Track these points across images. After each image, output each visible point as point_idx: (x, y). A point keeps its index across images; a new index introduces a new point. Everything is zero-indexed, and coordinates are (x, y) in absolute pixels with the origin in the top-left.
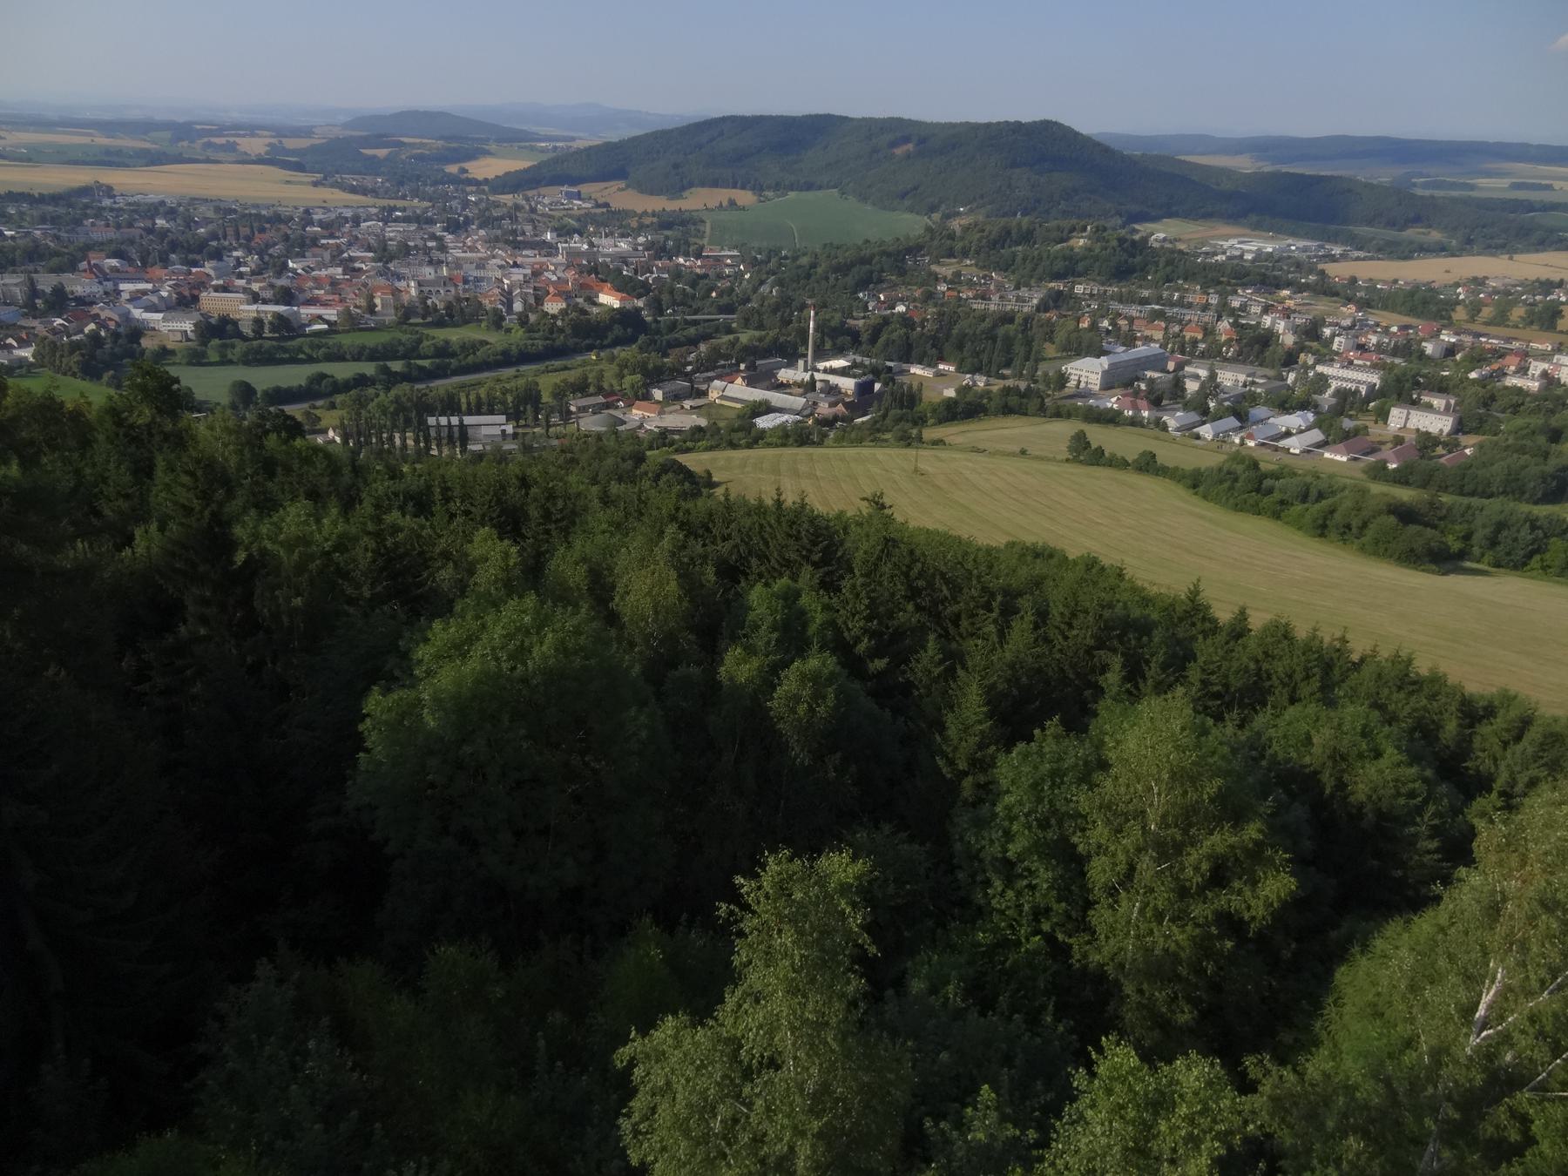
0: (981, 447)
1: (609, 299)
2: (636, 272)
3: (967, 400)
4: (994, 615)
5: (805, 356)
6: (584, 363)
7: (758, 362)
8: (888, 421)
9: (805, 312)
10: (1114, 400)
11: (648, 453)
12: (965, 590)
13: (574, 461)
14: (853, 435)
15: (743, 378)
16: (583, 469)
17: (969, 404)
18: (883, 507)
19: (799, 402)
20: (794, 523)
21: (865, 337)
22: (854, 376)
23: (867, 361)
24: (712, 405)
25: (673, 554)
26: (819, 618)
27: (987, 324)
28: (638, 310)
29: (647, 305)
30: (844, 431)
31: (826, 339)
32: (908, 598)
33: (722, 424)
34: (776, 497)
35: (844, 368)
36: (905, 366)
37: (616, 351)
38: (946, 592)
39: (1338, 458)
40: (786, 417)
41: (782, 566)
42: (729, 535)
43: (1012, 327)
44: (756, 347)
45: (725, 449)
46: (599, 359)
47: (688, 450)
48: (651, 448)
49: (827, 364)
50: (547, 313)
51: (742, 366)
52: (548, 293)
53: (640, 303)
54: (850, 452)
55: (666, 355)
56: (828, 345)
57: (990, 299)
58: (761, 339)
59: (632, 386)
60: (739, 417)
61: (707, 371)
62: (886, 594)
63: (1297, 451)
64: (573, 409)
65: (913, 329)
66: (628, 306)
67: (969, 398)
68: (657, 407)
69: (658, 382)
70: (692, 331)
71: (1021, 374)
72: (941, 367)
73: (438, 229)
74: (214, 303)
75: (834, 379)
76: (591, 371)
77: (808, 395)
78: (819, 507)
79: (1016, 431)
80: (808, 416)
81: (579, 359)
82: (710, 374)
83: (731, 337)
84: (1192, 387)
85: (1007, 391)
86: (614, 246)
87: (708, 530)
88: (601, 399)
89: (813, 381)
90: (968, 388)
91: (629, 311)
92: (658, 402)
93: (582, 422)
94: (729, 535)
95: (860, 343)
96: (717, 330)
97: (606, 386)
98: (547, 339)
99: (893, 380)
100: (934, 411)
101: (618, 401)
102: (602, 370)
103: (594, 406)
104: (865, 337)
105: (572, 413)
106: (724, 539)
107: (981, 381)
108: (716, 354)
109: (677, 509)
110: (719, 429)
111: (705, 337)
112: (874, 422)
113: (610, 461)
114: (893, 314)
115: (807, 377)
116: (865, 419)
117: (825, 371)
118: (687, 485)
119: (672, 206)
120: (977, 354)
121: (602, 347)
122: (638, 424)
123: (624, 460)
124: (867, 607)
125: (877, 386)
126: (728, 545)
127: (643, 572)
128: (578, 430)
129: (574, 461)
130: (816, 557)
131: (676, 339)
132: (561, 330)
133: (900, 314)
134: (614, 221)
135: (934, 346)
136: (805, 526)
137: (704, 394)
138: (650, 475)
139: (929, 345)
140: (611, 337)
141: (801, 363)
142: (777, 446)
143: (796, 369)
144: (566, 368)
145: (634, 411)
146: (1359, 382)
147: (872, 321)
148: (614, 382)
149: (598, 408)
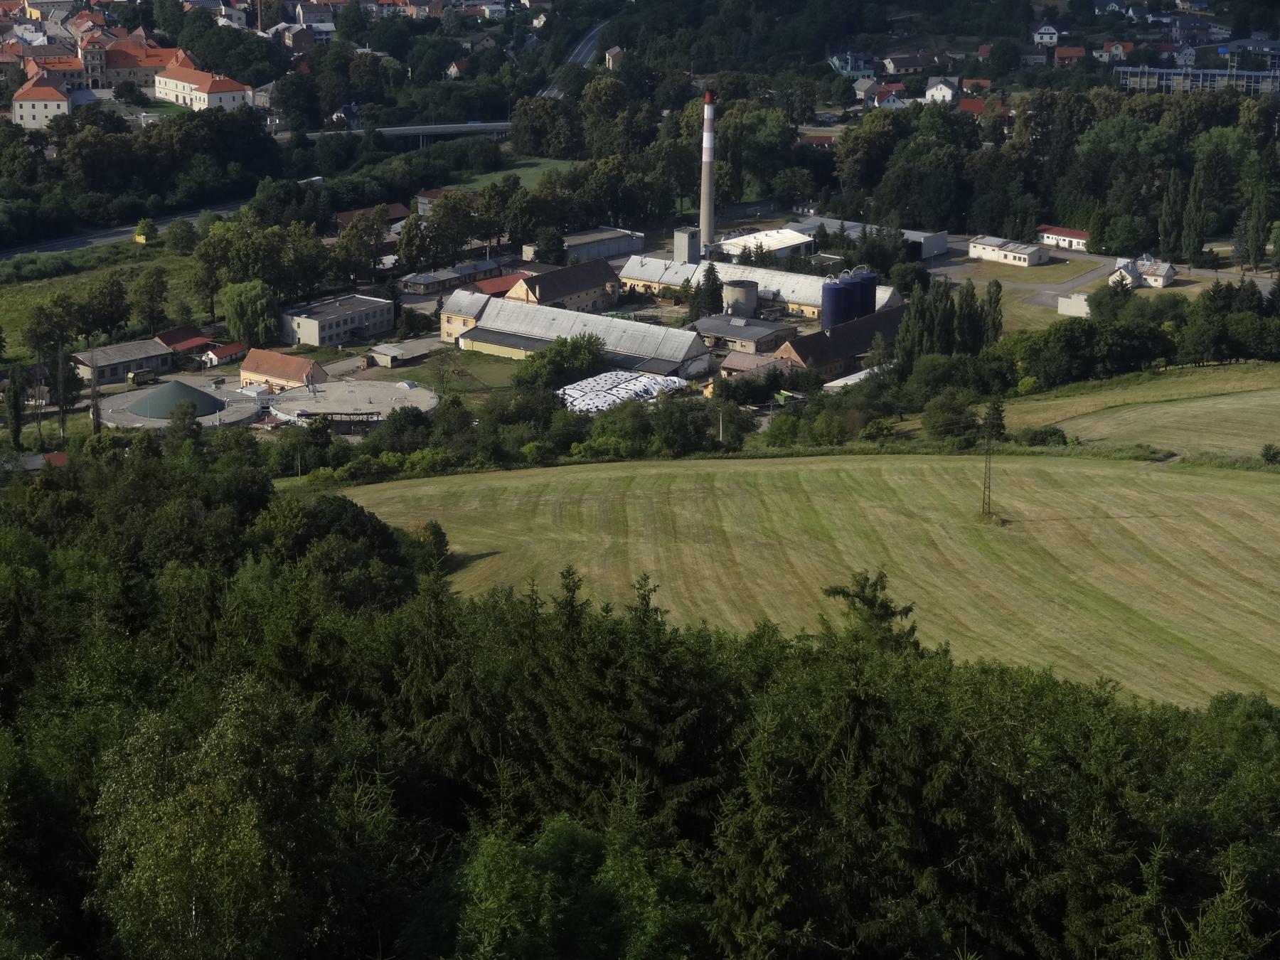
0: (1160, 444)
2: (251, 18)
3: (1121, 323)
4: (1149, 898)
5: (693, 220)
6: (117, 254)
7: (569, 241)
8: (912, 385)
9: (689, 109)
11: (279, 484)
12: (1074, 832)
13: (79, 509)
14: (819, 424)
15: (531, 283)
16: (103, 529)
17: (1126, 333)
18: (887, 612)
19: (678, 341)
20: (607, 662)
21: (845, 169)
22: (820, 271)
23: (854, 231)
24: (449, 353)
25: (253, 759)
26: (653, 919)
27: (1165, 127)
28: (253, 116)
29: (281, 100)
30: (798, 413)
31: (747, 176)
32: (918, 860)
33: (474, 403)
34: (562, 594)
35: (795, 249)
36: (954, 241)
37: (196, 222)
38: (1021, 839)
40: (643, 381)
41: (579, 776)
42: (443, 698)
43: (1231, 134)
44: (565, 201)
45: (482, 468)
46: (155, 243)
47: (386, 474)
48: (287, 470)
49: (750, 241)
50: (19, 130)
51: (528, 252)
52: (23, 78)
53: (259, 98)
54: (814, 468)
55: (327, 228)
56: (751, 193)
57: (1171, 63)
58: (575, 181)
59: (241, 312)
60: (520, 382)
61: (436, 266)
62: (844, 848)
64: (84, 372)
65: (974, 145)
66: (230, 104)
67: (1125, 318)
68: (306, 363)
69: (309, 298)
70: (397, 164)
71: (1261, 252)
72: (1050, 240)
75: (767, 280)
76: (133, 273)
77: (703, 322)
78: (676, 619)
79: (1253, 401)
80: (701, 377)
81: (101, 244)
82: (445, 274)
83: (498, 178)
85: (1223, 298)
87: (391, 686)
88: (157, 347)
89: (713, 285)
90: (1121, 292)
91: (231, 117)
92: (308, 350)
93: (107, 406)
94: (443, 698)
95: (835, 184)
96: (462, 161)
97: (171, 311)
98: (17, 194)
99: (924, 279)
100: (1034, 354)
101: (203, 349)
102: (161, 272)
103: (139, 364)
104: (845, 169)
105: (80, 383)
106: (433, 708)
107: (1155, 275)
108: (457, 217)
109: (304, 633)
110: (466, 418)
111: (430, 181)
112: (875, 387)
113: (173, 507)
114: (920, 107)
115: (697, 275)
116: (852, 380)
117: (746, 259)
118: (376, 565)
120: (1143, 205)
121: (163, 213)
122: (253, 408)
123: (208, 503)
124: (783, 886)
125: (883, 295)
126: (443, 723)
127: (168, 806)
128: (98, 426)
129: (79, 509)
130: (668, 753)
131: (355, 187)
132: (56, 171)
133: (939, 109)
135: (1028, 187)
136: (638, 665)
137: (429, 325)
138: (279, 541)
139: (1015, 186)
140: (184, 184)
141: (681, 240)
142: (618, 457)
143: (670, 254)
144: (67, 269)
145: (246, 376)
147: (867, 127)
148: (194, 302)
149: (149, 372)
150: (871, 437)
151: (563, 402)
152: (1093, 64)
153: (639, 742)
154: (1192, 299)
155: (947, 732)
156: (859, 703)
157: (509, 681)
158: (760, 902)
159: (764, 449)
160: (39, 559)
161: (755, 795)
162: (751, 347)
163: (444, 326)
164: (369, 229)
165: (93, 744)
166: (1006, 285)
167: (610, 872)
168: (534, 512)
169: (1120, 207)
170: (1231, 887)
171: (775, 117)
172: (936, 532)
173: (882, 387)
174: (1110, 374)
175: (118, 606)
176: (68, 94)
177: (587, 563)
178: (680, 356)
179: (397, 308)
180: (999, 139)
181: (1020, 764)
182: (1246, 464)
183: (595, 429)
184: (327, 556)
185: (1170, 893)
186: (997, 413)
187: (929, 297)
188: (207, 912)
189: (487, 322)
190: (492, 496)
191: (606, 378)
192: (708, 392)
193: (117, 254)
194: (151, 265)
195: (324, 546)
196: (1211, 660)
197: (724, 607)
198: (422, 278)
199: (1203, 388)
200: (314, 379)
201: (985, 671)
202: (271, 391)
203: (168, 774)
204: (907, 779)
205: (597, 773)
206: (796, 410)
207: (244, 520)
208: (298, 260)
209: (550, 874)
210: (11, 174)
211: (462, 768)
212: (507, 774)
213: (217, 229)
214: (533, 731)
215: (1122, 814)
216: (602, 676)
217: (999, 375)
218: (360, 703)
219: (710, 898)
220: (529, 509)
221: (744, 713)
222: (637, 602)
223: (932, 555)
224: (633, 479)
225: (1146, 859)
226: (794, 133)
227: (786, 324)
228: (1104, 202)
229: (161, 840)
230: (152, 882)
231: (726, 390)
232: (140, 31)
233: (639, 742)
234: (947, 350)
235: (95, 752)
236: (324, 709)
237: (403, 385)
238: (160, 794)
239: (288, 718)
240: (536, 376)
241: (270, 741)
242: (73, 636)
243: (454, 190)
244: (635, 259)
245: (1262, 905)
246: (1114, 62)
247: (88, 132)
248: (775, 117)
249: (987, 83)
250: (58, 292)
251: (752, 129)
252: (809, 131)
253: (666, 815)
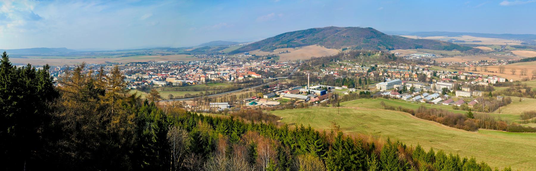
1: (254, 76)
5: (307, 85)
10: (390, 92)
36: (334, 87)
39: (446, 104)
63: (436, 103)
64: (244, 101)
73: (216, 64)
74: (169, 80)
84: (408, 88)
86: (254, 64)
90: (351, 92)
115: (308, 91)
119: (271, 54)
134: (257, 58)
143: (305, 88)
146: (447, 85)
178: (306, 98)
244: (301, 89)
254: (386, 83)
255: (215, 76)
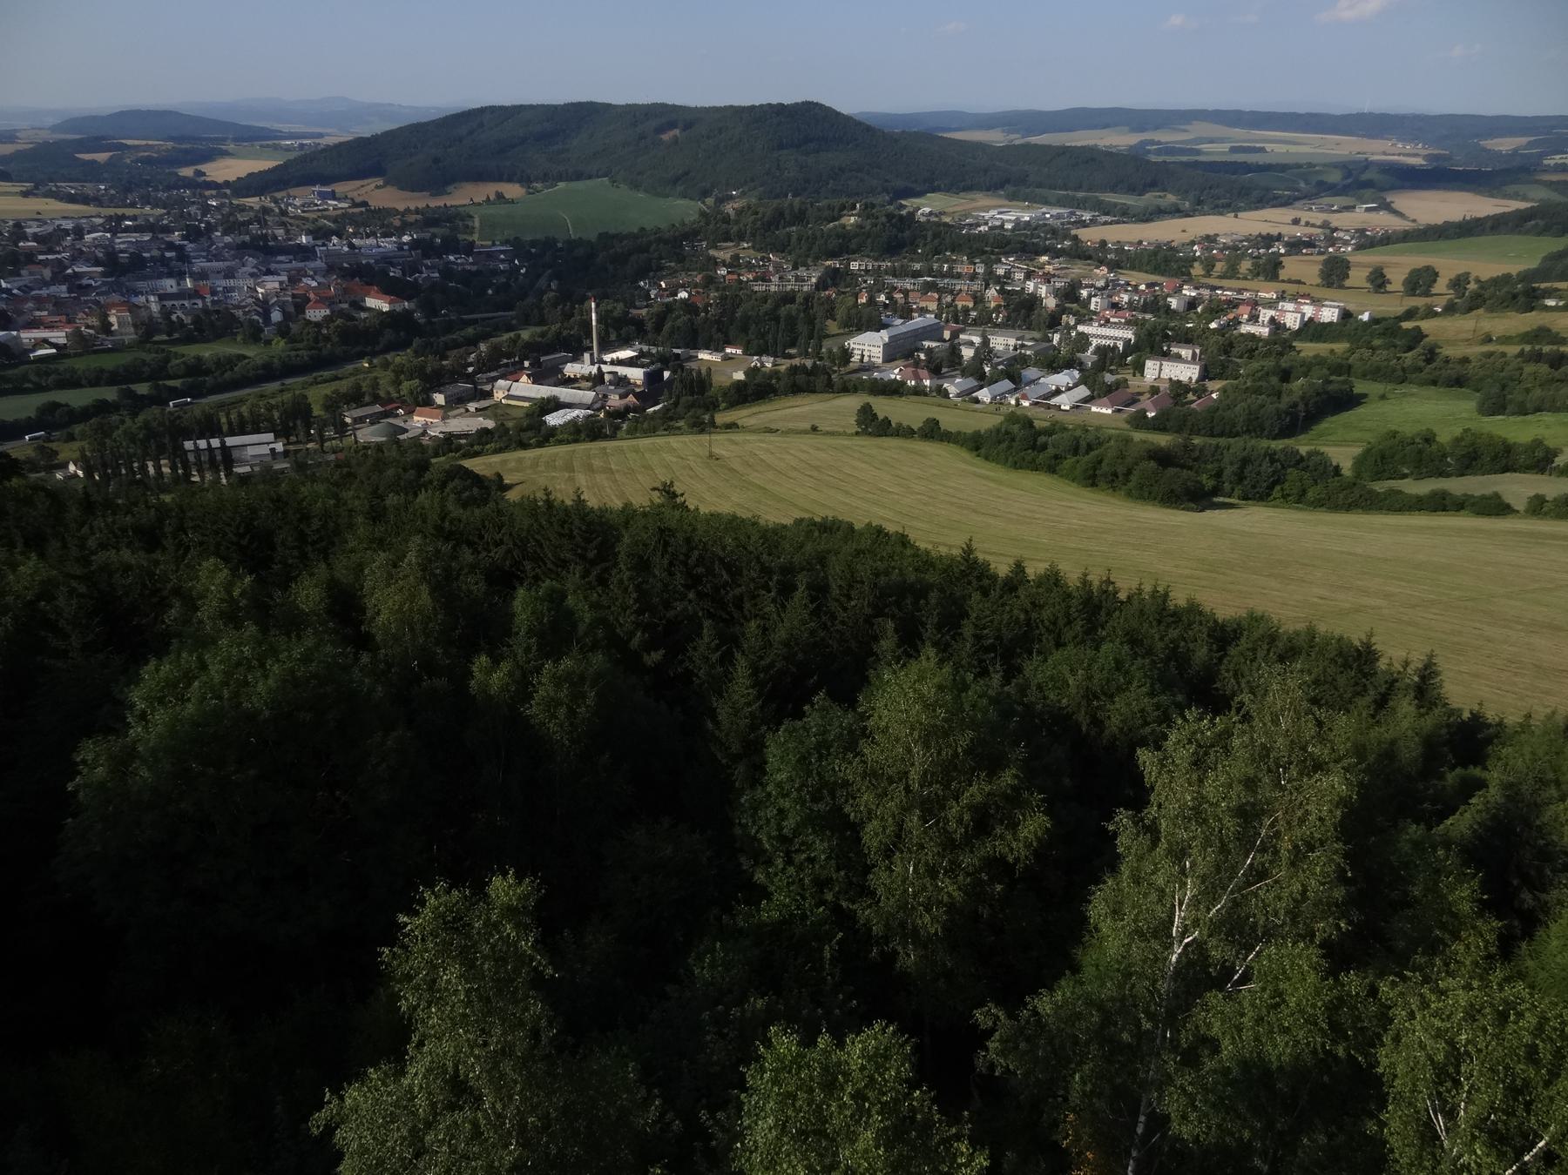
0: (774, 426)
5: (591, 348)
8: (680, 409)
10: (897, 371)
11: (434, 461)
12: (745, 572)
14: (645, 425)
15: (529, 376)
17: (758, 385)
18: (674, 495)
19: (589, 396)
20: (565, 522)
23: (654, 350)
24: (498, 405)
26: (588, 617)
27: (769, 305)
28: (407, 314)
30: (637, 422)
31: (611, 330)
32: (688, 587)
33: (510, 424)
34: (545, 498)
35: (632, 358)
36: (692, 352)
37: (388, 357)
39: (1104, 411)
40: (576, 412)
46: (372, 367)
47: (477, 454)
48: (436, 455)
49: (614, 356)
51: (526, 364)
54: (644, 442)
56: (613, 337)
57: (770, 281)
58: (543, 335)
60: (527, 415)
63: (1067, 408)
64: (348, 420)
65: (697, 315)
66: (398, 308)
67: (759, 379)
72: (728, 350)
75: (622, 371)
76: (365, 379)
77: (598, 388)
78: (592, 502)
79: (806, 409)
80: (599, 410)
81: (350, 367)
83: (512, 334)
84: (967, 353)
85: (794, 370)
87: (481, 537)
88: (378, 408)
89: (601, 373)
91: (399, 313)
92: (440, 407)
93: (359, 433)
95: (646, 332)
97: (382, 394)
98: (313, 348)
99: (682, 368)
100: (725, 394)
101: (397, 408)
102: (376, 378)
103: (370, 416)
104: (649, 326)
106: (497, 544)
109: (443, 519)
110: (507, 430)
111: (484, 337)
112: (666, 410)
113: (390, 472)
115: (594, 370)
117: (613, 363)
118: (475, 490)
120: (762, 335)
121: (374, 354)
122: (421, 431)
123: (405, 470)
124: (636, 601)
125: (666, 374)
126: (502, 550)
128: (356, 442)
129: (351, 475)
130: (591, 554)
131: (454, 340)
132: (327, 338)
135: (719, 330)
136: (577, 522)
137: (490, 394)
139: (714, 330)
141: (587, 356)
142: (569, 442)
143: (583, 362)
144: (336, 378)
145: (416, 418)
147: (655, 310)
148: (391, 389)
150: (665, 430)
151: (545, 422)
152: (741, 282)
153: (579, 551)
154: (782, 371)
155: (696, 539)
156: (661, 531)
157: (528, 531)
158: (628, 607)
159: (625, 436)
160: (336, 496)
161: (623, 567)
162: (617, 397)
163: (495, 394)
164: (461, 357)
165: (360, 568)
166: (713, 369)
167: (570, 601)
168: (537, 466)
169: (753, 337)
170: (801, 588)
171: (620, 306)
172: (692, 464)
173: (668, 410)
174: (753, 401)
175: (368, 513)
176: (329, 306)
177: (560, 484)
179: (475, 388)
180: (707, 312)
181: (724, 548)
182: (805, 432)
183: (559, 432)
184: (455, 488)
185: (780, 592)
186: (712, 417)
187: (684, 374)
188: (412, 629)
189: (513, 392)
190: (520, 460)
191: (561, 412)
192: (602, 415)
193: (357, 371)
194: (372, 375)
195: (454, 484)
196: (795, 505)
197: (613, 497)
198: (485, 376)
199: (788, 405)
200: (444, 418)
201: (712, 515)
202: (427, 424)
203: (390, 576)
204: (682, 557)
205: (564, 564)
206: (636, 420)
207: (420, 476)
208: (433, 371)
209: (546, 603)
210: (308, 340)
211: (511, 566)
212: (529, 567)
213: (398, 360)
214: (538, 550)
215: (762, 564)
216: (563, 528)
217: (712, 403)
218: (470, 544)
219: (609, 607)
220: (535, 463)
221: (618, 539)
222: (576, 498)
223: (691, 473)
224: (574, 451)
225: (771, 579)
226: (628, 313)
227: (630, 387)
228: (747, 334)
229: (390, 603)
230: (388, 619)
231: (608, 414)
232: (357, 279)
233: (579, 551)
234: (692, 394)
235: (362, 571)
236: (454, 548)
237: (481, 419)
238: (388, 585)
239: (438, 551)
240: (534, 413)
241: (430, 561)
242: (351, 526)
243: (493, 340)
245: (814, 593)
246: (749, 280)
247: (339, 321)
248: (620, 306)
249: (701, 290)
250: (334, 388)
251: (611, 311)
252: (634, 312)
253: (592, 578)
254: (884, 335)
255: (186, 303)
